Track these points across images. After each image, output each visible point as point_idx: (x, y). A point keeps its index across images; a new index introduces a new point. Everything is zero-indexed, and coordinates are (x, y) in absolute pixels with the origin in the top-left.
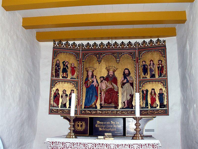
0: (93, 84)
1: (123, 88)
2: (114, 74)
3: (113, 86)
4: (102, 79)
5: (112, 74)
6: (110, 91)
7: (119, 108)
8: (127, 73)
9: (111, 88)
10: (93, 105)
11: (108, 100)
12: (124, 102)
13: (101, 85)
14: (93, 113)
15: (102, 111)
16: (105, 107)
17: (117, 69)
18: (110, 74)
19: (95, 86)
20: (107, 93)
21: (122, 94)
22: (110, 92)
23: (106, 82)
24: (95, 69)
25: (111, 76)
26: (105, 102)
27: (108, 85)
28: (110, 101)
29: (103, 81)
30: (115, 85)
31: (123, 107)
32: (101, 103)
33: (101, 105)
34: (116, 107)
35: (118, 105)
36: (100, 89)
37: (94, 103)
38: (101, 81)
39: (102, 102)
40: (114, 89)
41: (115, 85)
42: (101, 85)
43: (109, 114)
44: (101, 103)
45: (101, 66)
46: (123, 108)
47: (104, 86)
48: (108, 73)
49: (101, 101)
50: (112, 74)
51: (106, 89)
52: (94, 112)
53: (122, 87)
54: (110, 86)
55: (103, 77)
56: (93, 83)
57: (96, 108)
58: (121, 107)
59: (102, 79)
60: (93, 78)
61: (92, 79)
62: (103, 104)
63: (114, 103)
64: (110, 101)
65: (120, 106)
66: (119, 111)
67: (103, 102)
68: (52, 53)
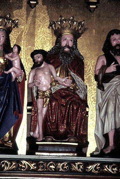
0: (10, 74)
1: (103, 90)
2: (76, 46)
3: (74, 82)
4: (39, 58)
5: (71, 44)
6: (64, 97)
7: (88, 155)
8: (69, 47)
9: (68, 87)
10: (6, 142)
11: (57, 128)
12: (106, 136)
13: (35, 77)
14: (6, 168)
15: (36, 162)
16: (47, 149)
17: (85, 29)
18: (64, 44)
19: (16, 79)
20: (54, 104)
21: (99, 109)
22: (63, 100)
23: (51, 67)
24: (16, 25)
25: (67, 49)
26: (46, 134)
27: (59, 79)
28: (62, 131)
29: (41, 63)
30: (80, 79)
31: (102, 151)
32: (32, 134)
33: (31, 140)
34: (81, 150)
35: (88, 143)
36: (30, 90)
37: (10, 133)
38: (36, 66)
39: (37, 132)
40: (77, 92)
41: (78, 79)
42: (35, 77)
43: (62, 172)
44: (32, 134)
45: (34, 17)
46: (102, 154)
47: (46, 80)
48: (58, 42)
49: (31, 127)
50: (71, 44)
51: (50, 89)
52: (12, 164)
53: (100, 87)
54: (65, 82)
55: (42, 52)
56: (11, 70)
57: (14, 150)
58: (97, 150)
59: (39, 59)
60: (10, 54)
61: (7, 56)
62: (41, 139)
63: (76, 136)
64: (62, 129)
65: (92, 147)
66: (92, 163)
67: (38, 132)
68: (20, 128)
